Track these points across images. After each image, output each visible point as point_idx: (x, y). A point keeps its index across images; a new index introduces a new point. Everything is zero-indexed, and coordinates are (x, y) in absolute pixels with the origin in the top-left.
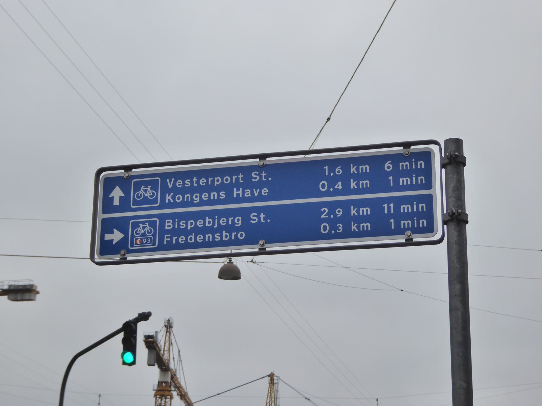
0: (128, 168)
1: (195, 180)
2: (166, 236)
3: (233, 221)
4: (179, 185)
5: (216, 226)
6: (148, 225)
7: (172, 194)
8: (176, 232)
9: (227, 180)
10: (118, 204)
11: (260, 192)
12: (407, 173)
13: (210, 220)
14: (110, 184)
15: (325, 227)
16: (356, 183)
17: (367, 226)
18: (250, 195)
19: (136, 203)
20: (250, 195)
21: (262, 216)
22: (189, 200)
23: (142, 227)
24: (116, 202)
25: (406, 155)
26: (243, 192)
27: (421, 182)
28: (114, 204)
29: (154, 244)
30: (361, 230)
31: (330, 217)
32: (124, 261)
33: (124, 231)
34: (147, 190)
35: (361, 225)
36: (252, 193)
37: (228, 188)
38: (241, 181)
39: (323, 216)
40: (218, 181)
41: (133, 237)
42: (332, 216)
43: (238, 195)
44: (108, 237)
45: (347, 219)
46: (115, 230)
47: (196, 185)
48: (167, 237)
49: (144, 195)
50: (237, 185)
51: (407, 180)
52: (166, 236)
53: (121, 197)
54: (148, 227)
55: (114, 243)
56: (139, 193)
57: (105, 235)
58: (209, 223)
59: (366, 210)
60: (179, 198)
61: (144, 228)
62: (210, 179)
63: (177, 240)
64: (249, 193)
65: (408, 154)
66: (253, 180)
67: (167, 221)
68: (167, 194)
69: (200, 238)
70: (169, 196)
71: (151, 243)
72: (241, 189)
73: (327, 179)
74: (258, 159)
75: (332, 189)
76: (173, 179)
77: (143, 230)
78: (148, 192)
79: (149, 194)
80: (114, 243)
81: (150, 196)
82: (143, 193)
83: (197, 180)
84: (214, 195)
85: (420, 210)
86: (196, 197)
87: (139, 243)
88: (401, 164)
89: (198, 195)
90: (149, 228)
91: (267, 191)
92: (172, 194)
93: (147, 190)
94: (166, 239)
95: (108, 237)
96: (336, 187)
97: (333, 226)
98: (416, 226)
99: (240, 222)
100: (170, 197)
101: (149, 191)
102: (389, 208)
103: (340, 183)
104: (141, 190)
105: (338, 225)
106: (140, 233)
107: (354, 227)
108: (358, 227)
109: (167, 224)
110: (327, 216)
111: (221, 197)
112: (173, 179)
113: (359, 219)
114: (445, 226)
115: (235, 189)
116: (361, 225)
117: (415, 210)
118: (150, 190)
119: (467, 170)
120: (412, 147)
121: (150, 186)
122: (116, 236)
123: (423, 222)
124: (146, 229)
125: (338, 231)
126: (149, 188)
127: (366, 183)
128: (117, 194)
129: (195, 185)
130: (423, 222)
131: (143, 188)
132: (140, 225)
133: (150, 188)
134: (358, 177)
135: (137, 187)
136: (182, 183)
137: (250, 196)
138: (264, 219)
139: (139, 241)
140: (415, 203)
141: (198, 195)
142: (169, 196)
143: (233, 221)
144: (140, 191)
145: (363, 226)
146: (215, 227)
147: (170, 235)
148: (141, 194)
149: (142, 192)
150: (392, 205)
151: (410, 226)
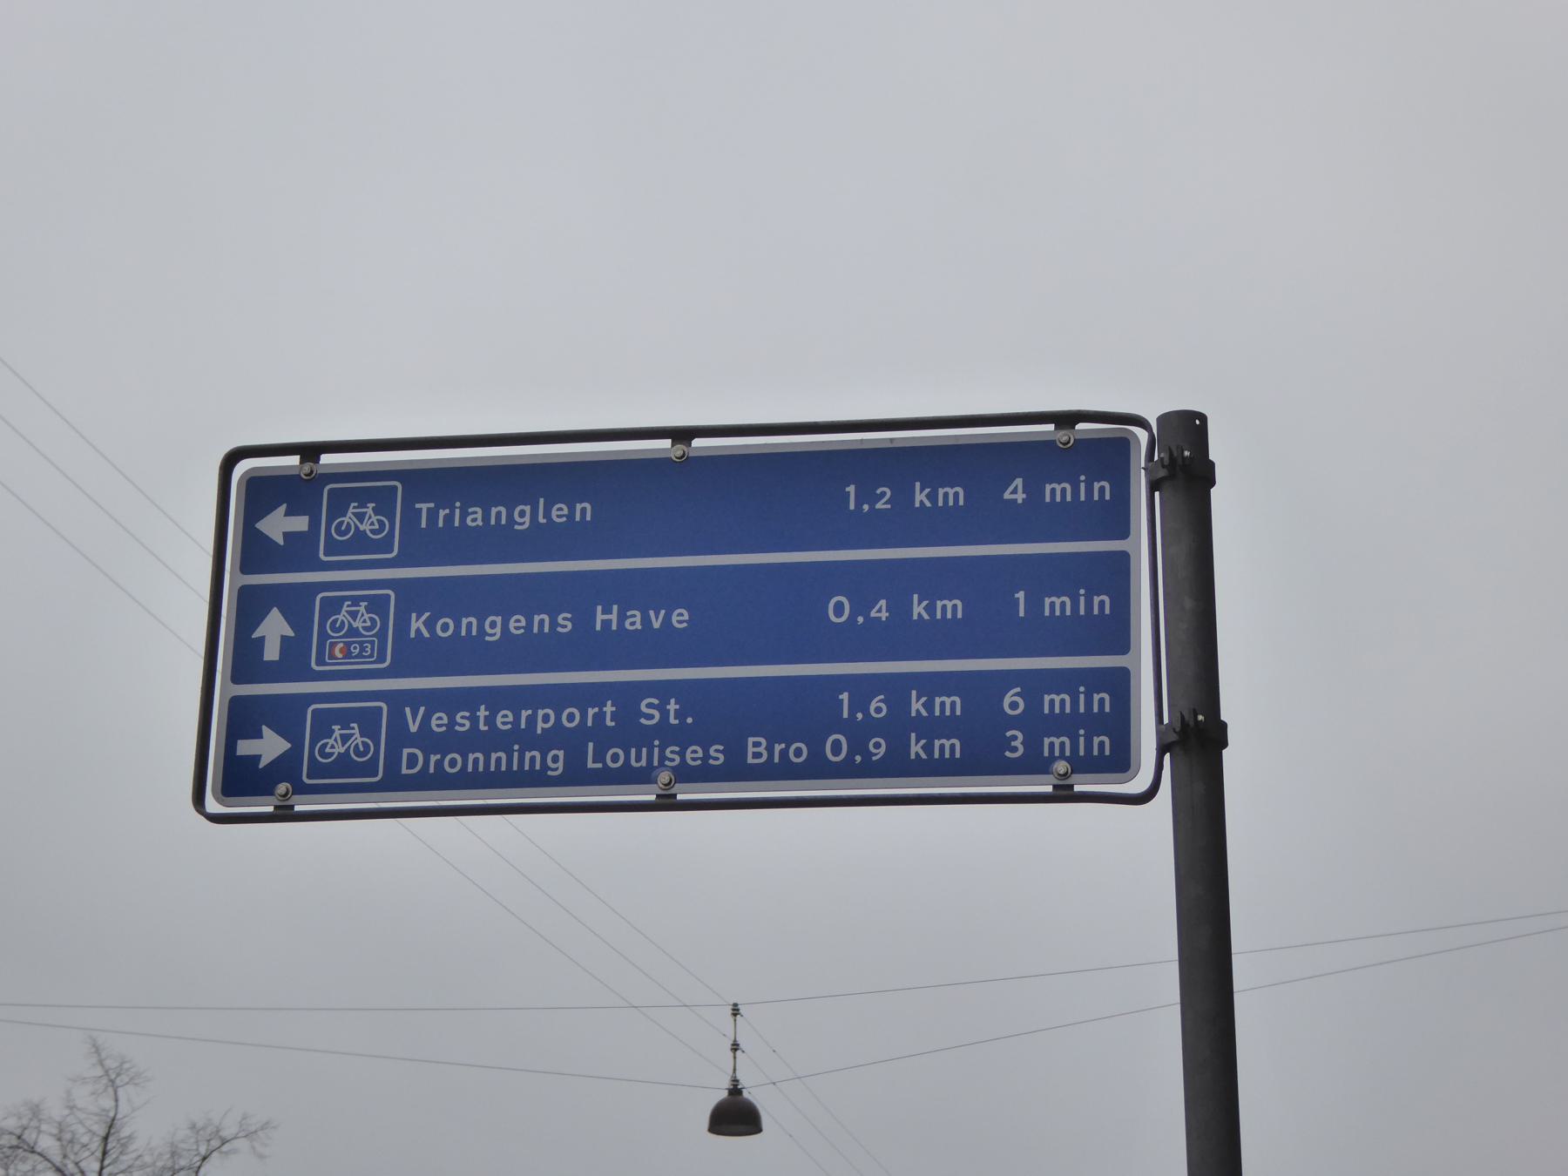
0: (310, 451)
1: (482, 713)
4: (438, 726)
6: (356, 731)
9: (571, 717)
10: (276, 658)
14: (263, 493)
15: (837, 745)
16: (929, 492)
17: (953, 704)
18: (638, 626)
19: (332, 548)
20: (638, 626)
21: (672, 706)
22: (474, 633)
23: (341, 735)
24: (272, 653)
25: (1061, 446)
26: (622, 617)
27: (1099, 496)
28: (266, 658)
29: (381, 659)
30: (939, 616)
32: (285, 814)
34: (358, 611)
35: (939, 604)
36: (646, 620)
37: (572, 742)
38: (610, 723)
40: (546, 718)
41: (323, 636)
43: (607, 624)
44: (245, 747)
45: (898, 726)
46: (281, 541)
47: (486, 728)
49: (357, 527)
50: (598, 731)
51: (1063, 491)
53: (284, 639)
54: (357, 735)
55: (283, 507)
56: (342, 522)
59: (949, 704)
60: (445, 627)
61: (345, 739)
62: (525, 714)
64: (638, 619)
65: (1069, 442)
66: (643, 721)
68: (414, 615)
72: (615, 608)
73: (847, 727)
74: (670, 440)
75: (861, 619)
76: (422, 709)
77: (343, 746)
78: (370, 522)
79: (370, 525)
80: (283, 507)
82: (349, 622)
83: (487, 713)
84: (542, 622)
85: (1096, 612)
87: (340, 656)
88: (1048, 488)
89: (499, 620)
90: (359, 740)
91: (686, 617)
93: (358, 611)
95: (245, 747)
96: (873, 614)
97: (858, 745)
98: (1082, 710)
100: (420, 624)
101: (370, 517)
104: (343, 612)
106: (332, 754)
107: (916, 749)
111: (560, 629)
112: (422, 709)
113: (931, 728)
114: (1157, 494)
115: (599, 608)
116: (939, 604)
117: (1082, 710)
118: (373, 515)
119: (1230, 758)
120: (1080, 426)
121: (366, 603)
122: (269, 746)
123: (1102, 742)
124: (350, 742)
126: (371, 508)
127: (956, 495)
128: (274, 629)
129: (483, 728)
130: (1102, 742)
132: (333, 731)
133: (373, 509)
136: (445, 721)
138: (678, 714)
140: (1082, 689)
141: (499, 620)
144: (339, 614)
145: (946, 495)
148: (342, 620)
149: (344, 616)
151: (1068, 753)
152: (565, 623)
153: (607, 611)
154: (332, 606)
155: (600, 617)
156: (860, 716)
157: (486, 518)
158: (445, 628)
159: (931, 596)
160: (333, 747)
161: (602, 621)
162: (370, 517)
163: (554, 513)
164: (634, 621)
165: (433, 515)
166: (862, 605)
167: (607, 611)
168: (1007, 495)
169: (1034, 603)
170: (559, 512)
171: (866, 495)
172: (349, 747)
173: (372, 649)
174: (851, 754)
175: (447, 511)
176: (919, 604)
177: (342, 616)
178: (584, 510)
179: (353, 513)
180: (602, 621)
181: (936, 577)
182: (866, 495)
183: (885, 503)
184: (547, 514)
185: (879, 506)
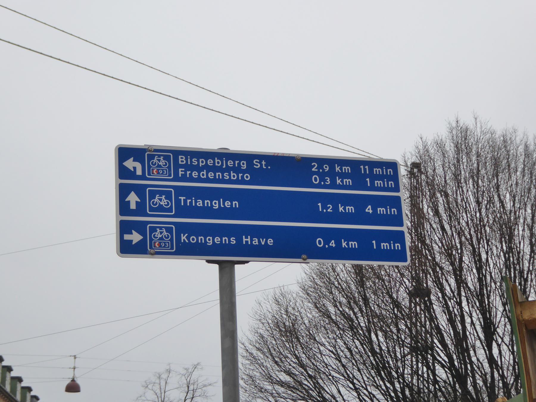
2: (180, 170)
3: (239, 164)
5: (224, 167)
6: (164, 231)
7: (186, 235)
8: (189, 167)
10: (135, 208)
11: (266, 242)
12: (381, 177)
13: (219, 160)
18: (257, 243)
19: (151, 209)
20: (257, 243)
24: (133, 206)
26: (252, 241)
28: (131, 208)
31: (319, 170)
33: (142, 232)
36: (259, 241)
39: (313, 170)
41: (151, 240)
42: (321, 170)
43: (247, 242)
44: (127, 237)
45: (332, 174)
48: (182, 171)
49: (159, 203)
52: (180, 170)
54: (165, 232)
56: (154, 201)
57: (125, 239)
58: (218, 163)
61: (161, 233)
63: (191, 174)
64: (257, 241)
66: (255, 166)
67: (180, 157)
68: (182, 235)
69: (211, 175)
70: (184, 236)
71: (169, 247)
72: (249, 237)
77: (161, 235)
81: (165, 205)
86: (209, 240)
87: (156, 173)
89: (211, 238)
90: (166, 234)
91: (272, 242)
92: (186, 235)
94: (180, 173)
95: (127, 237)
96: (330, 245)
97: (322, 179)
99: (245, 165)
100: (184, 237)
101: (162, 161)
102: (365, 169)
103: (333, 241)
105: (326, 178)
106: (158, 237)
107: (339, 181)
108: (342, 181)
109: (180, 160)
110: (317, 170)
115: (244, 237)
122: (135, 237)
125: (326, 183)
131: (158, 196)
132: (157, 230)
133: (165, 197)
134: (343, 176)
135: (153, 195)
137: (258, 244)
139: (156, 172)
141: (211, 238)
142: (184, 236)
143: (239, 164)
144: (154, 159)
146: (223, 167)
147: (184, 169)
148: (156, 202)
150: (367, 167)
152: (233, 241)
153: (246, 238)
154: (153, 230)
155: (244, 240)
156: (327, 246)
157: (203, 203)
158: (193, 239)
159: (348, 240)
160: (157, 235)
161: (245, 241)
162: (164, 200)
163: (226, 204)
164: (256, 242)
165: (185, 201)
166: (327, 242)
167: (246, 238)
168: (367, 211)
169: (378, 245)
170: (228, 204)
171: (324, 207)
172: (163, 236)
173: (169, 245)
174: (320, 182)
175: (190, 200)
176: (344, 243)
177: (155, 160)
178: (236, 203)
179: (158, 198)
180: (245, 241)
181: (350, 235)
182: (324, 207)
183: (331, 210)
184: (224, 204)
185: (329, 210)
